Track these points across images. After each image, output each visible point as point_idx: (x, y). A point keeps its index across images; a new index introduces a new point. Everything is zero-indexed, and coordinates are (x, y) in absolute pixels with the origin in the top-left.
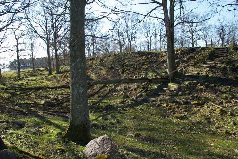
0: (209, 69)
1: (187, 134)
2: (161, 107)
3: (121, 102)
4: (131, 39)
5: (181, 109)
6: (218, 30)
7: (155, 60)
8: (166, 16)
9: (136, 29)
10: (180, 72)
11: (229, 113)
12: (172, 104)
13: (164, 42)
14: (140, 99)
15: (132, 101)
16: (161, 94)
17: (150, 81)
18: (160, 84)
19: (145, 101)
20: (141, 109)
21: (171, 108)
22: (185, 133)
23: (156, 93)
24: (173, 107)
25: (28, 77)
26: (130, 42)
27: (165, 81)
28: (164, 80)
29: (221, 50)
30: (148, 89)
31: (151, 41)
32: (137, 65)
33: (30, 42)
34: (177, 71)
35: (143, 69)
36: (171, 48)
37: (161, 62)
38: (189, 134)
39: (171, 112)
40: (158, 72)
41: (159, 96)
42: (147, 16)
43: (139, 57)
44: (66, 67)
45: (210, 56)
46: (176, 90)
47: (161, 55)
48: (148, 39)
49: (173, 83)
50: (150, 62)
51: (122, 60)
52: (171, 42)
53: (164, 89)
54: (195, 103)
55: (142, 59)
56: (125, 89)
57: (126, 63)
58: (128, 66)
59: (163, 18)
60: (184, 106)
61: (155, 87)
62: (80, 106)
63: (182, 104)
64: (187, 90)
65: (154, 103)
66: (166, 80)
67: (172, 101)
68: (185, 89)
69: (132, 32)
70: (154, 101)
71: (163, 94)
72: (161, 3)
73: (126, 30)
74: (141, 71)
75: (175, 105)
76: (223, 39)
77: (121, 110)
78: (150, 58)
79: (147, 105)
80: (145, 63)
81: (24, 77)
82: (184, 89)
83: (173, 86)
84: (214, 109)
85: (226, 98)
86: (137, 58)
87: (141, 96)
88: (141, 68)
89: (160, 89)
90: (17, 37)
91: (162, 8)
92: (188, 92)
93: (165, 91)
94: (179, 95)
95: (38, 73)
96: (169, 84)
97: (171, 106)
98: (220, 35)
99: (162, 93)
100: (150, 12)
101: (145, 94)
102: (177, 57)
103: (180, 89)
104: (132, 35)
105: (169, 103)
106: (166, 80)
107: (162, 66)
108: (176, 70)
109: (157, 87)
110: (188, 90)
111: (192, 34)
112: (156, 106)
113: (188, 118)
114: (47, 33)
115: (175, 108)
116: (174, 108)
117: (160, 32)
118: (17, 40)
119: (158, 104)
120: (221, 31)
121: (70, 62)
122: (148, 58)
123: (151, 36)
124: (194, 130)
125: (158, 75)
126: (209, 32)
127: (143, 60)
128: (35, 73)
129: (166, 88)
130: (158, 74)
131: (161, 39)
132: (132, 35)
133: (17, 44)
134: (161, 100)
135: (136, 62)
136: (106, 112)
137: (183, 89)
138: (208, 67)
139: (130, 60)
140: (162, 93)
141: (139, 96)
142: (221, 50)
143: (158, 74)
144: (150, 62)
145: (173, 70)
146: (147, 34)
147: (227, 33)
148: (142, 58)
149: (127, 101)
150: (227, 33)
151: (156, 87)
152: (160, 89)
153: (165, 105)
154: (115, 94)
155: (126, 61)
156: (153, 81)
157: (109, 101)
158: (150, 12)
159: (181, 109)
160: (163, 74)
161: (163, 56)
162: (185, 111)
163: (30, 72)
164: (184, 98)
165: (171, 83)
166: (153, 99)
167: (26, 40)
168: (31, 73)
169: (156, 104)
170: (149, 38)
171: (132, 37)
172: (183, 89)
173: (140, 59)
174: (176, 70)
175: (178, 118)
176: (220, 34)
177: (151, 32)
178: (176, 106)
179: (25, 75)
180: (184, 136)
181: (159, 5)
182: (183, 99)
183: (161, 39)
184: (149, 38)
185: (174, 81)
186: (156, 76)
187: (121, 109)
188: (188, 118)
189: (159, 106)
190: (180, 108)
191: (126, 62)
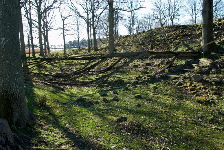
1: (205, 127)
2: (182, 86)
3: (137, 78)
4: (174, 17)
5: (209, 91)
7: (190, 33)
9: (180, 5)
10: (219, 44)
12: (197, 84)
14: (158, 76)
15: (149, 77)
16: (187, 71)
17: (179, 55)
18: (190, 60)
19: (165, 78)
20: (154, 87)
21: (194, 88)
22: (202, 126)
23: (180, 70)
24: (198, 87)
25: (73, 55)
26: (172, 20)
27: (196, 56)
28: (196, 55)
30: (173, 65)
31: (196, 18)
32: (168, 40)
33: (77, 24)
34: (214, 43)
35: (174, 43)
36: (207, 13)
37: (197, 36)
38: (208, 127)
39: (193, 94)
40: (190, 46)
41: (184, 74)
43: (173, 31)
44: (104, 45)
46: (208, 66)
47: (198, 27)
48: (193, 17)
49: (207, 58)
50: (184, 36)
51: (155, 36)
52: (208, 5)
53: (192, 65)
55: (176, 33)
56: (148, 64)
57: (158, 38)
58: (158, 41)
60: (215, 87)
61: (183, 62)
65: (175, 81)
66: (199, 55)
67: (199, 79)
68: (222, 66)
69: (175, 9)
70: (175, 78)
71: (190, 71)
73: (168, 8)
74: (172, 46)
75: (202, 85)
77: (130, 86)
78: (185, 32)
79: (165, 83)
80: (178, 37)
81: (70, 54)
82: (220, 66)
83: (205, 62)
86: (171, 32)
88: (172, 42)
89: (189, 65)
90: (64, 19)
93: (194, 68)
94: (211, 72)
95: (82, 51)
96: (201, 60)
97: (195, 86)
99: (188, 70)
101: (167, 70)
102: (219, 27)
103: (213, 65)
104: (174, 12)
105: (195, 82)
106: (199, 55)
107: (197, 39)
108: (212, 42)
109: (185, 62)
112: (176, 84)
113: (216, 104)
114: (87, 13)
115: (200, 89)
116: (200, 88)
118: (63, 21)
119: (178, 82)
121: (152, 51)
122: (182, 32)
123: (196, 13)
124: (219, 123)
125: (189, 50)
127: (176, 34)
128: (80, 51)
129: (195, 64)
130: (189, 49)
132: (174, 12)
133: (64, 25)
134: (185, 78)
135: (169, 37)
136: (111, 88)
137: (218, 66)
139: (162, 34)
140: (188, 70)
141: (160, 73)
143: (189, 49)
144: (184, 36)
146: (192, 11)
148: (176, 32)
149: (143, 77)
151: (183, 63)
152: (189, 65)
153: (188, 84)
154: (135, 70)
155: (158, 36)
156: (181, 55)
157: (121, 76)
159: (209, 91)
160: (195, 49)
162: (215, 94)
163: (76, 50)
164: (216, 77)
165: (204, 58)
166: (175, 76)
167: (71, 21)
168: (77, 51)
169: (177, 82)
170: (194, 15)
171: (174, 15)
172: (218, 66)
173: (174, 33)
174: (212, 42)
175: (199, 102)
177: (197, 8)
178: (203, 86)
179: (71, 53)
180: (197, 131)
182: (216, 78)
184: (194, 15)
185: (207, 55)
186: (187, 50)
187: (131, 85)
188: (216, 104)
189: (179, 85)
190: (208, 89)
191: (157, 37)
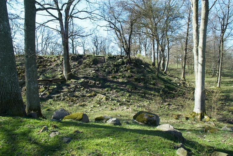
0: (94, 71)
6: (93, 39)
8: (62, 29)
11: (111, 99)
12: (73, 98)
13: (46, 46)
29: (100, 57)
34: (71, 73)
36: (66, 55)
42: (42, 25)
45: (94, 62)
52: (66, 50)
54: (89, 96)
59: (60, 30)
62: (35, 96)
63: (79, 97)
64: (81, 87)
67: (73, 95)
68: (80, 87)
72: (58, 18)
75: (76, 98)
76: (97, 47)
84: (101, 98)
85: (108, 91)
87: (45, 94)
91: (58, 21)
92: (82, 88)
98: (95, 43)
100: (46, 23)
110: (82, 87)
111: (73, 41)
117: (41, 35)
120: (96, 40)
126: (86, 40)
131: (42, 42)
138: (94, 70)
142: (100, 57)
145: (68, 72)
147: (99, 42)
150: (99, 42)
158: (46, 23)
161: (56, 61)
169: (61, 99)
174: (70, 73)
176: (95, 42)
178: (76, 99)
181: (56, 19)
183: (42, 42)
